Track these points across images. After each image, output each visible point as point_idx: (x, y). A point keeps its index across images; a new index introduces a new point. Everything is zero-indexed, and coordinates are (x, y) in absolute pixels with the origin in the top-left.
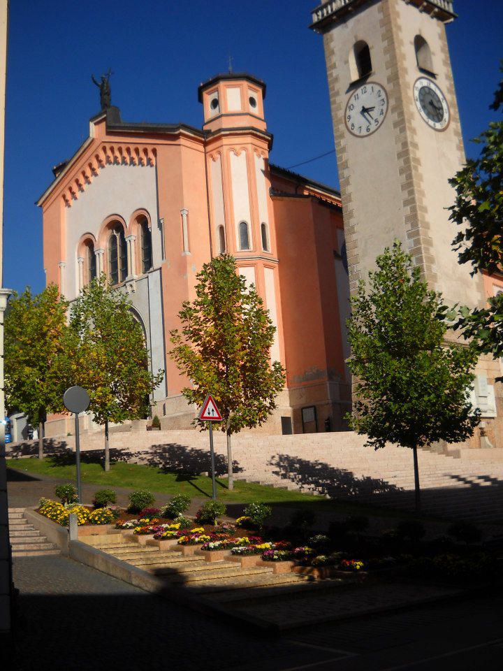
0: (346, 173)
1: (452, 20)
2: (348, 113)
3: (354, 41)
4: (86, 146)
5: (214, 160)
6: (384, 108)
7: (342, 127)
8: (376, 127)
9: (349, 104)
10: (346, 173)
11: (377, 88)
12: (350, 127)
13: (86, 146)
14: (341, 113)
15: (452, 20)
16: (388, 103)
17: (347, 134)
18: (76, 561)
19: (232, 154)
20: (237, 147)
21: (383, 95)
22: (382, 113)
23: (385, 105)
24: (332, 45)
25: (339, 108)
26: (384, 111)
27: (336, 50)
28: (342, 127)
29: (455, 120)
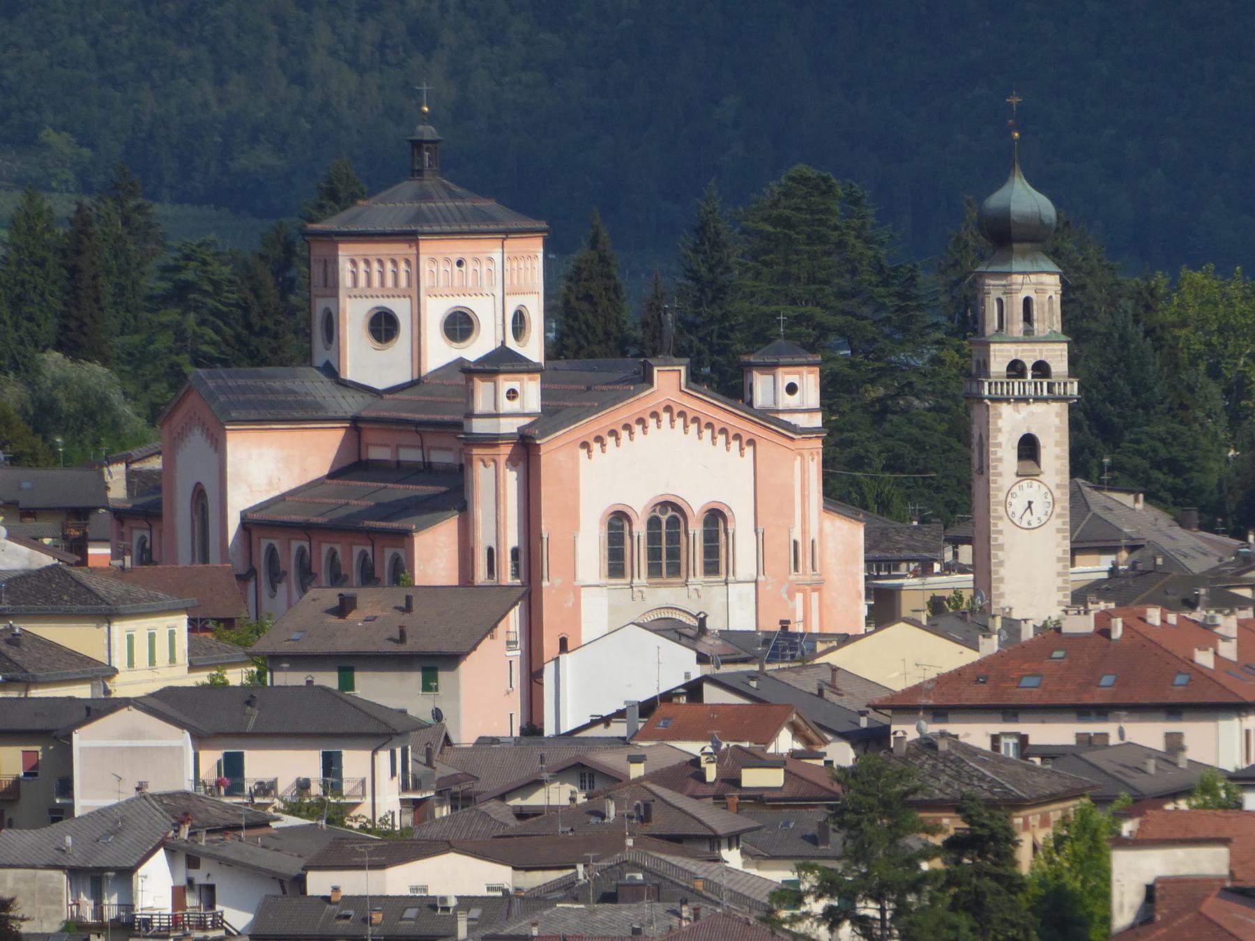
0: (1001, 554)
1: (229, 565)
2: (1009, 499)
3: (1025, 432)
4: (772, 427)
5: (485, 466)
6: (1050, 510)
7: (1001, 510)
8: (1038, 525)
9: (1011, 492)
10: (1001, 554)
11: (1044, 489)
12: (1010, 514)
13: (772, 427)
14: (1002, 496)
15: (229, 565)
16: (1053, 507)
17: (1006, 518)
18: (538, 897)
19: (481, 464)
20: (486, 458)
21: (1050, 499)
22: (1046, 514)
23: (1051, 508)
24: (1000, 423)
25: (1000, 489)
26: (1049, 514)
27: (1004, 430)
28: (1001, 510)
29: (998, 503)
